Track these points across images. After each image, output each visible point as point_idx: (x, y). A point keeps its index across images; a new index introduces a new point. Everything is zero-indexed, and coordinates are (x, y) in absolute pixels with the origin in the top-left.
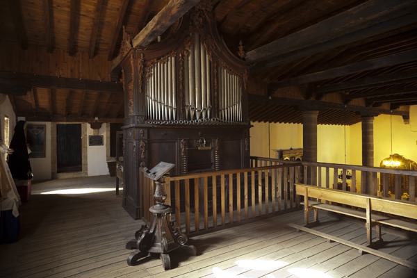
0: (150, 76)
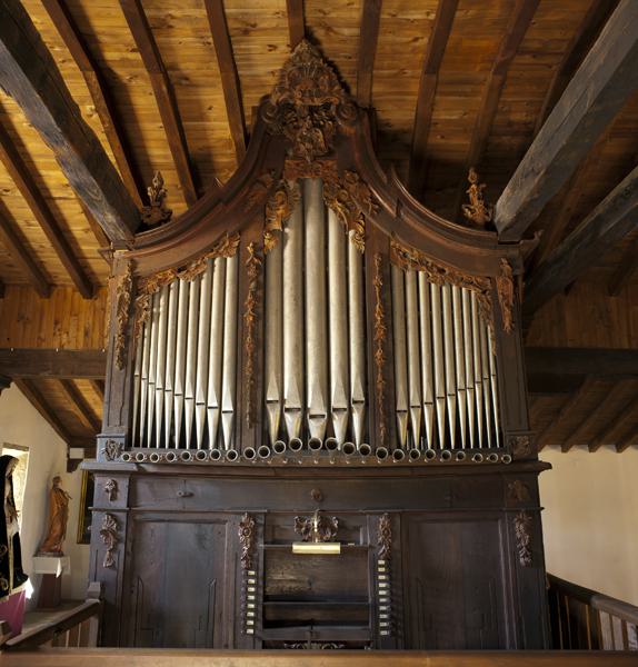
0: (153, 318)
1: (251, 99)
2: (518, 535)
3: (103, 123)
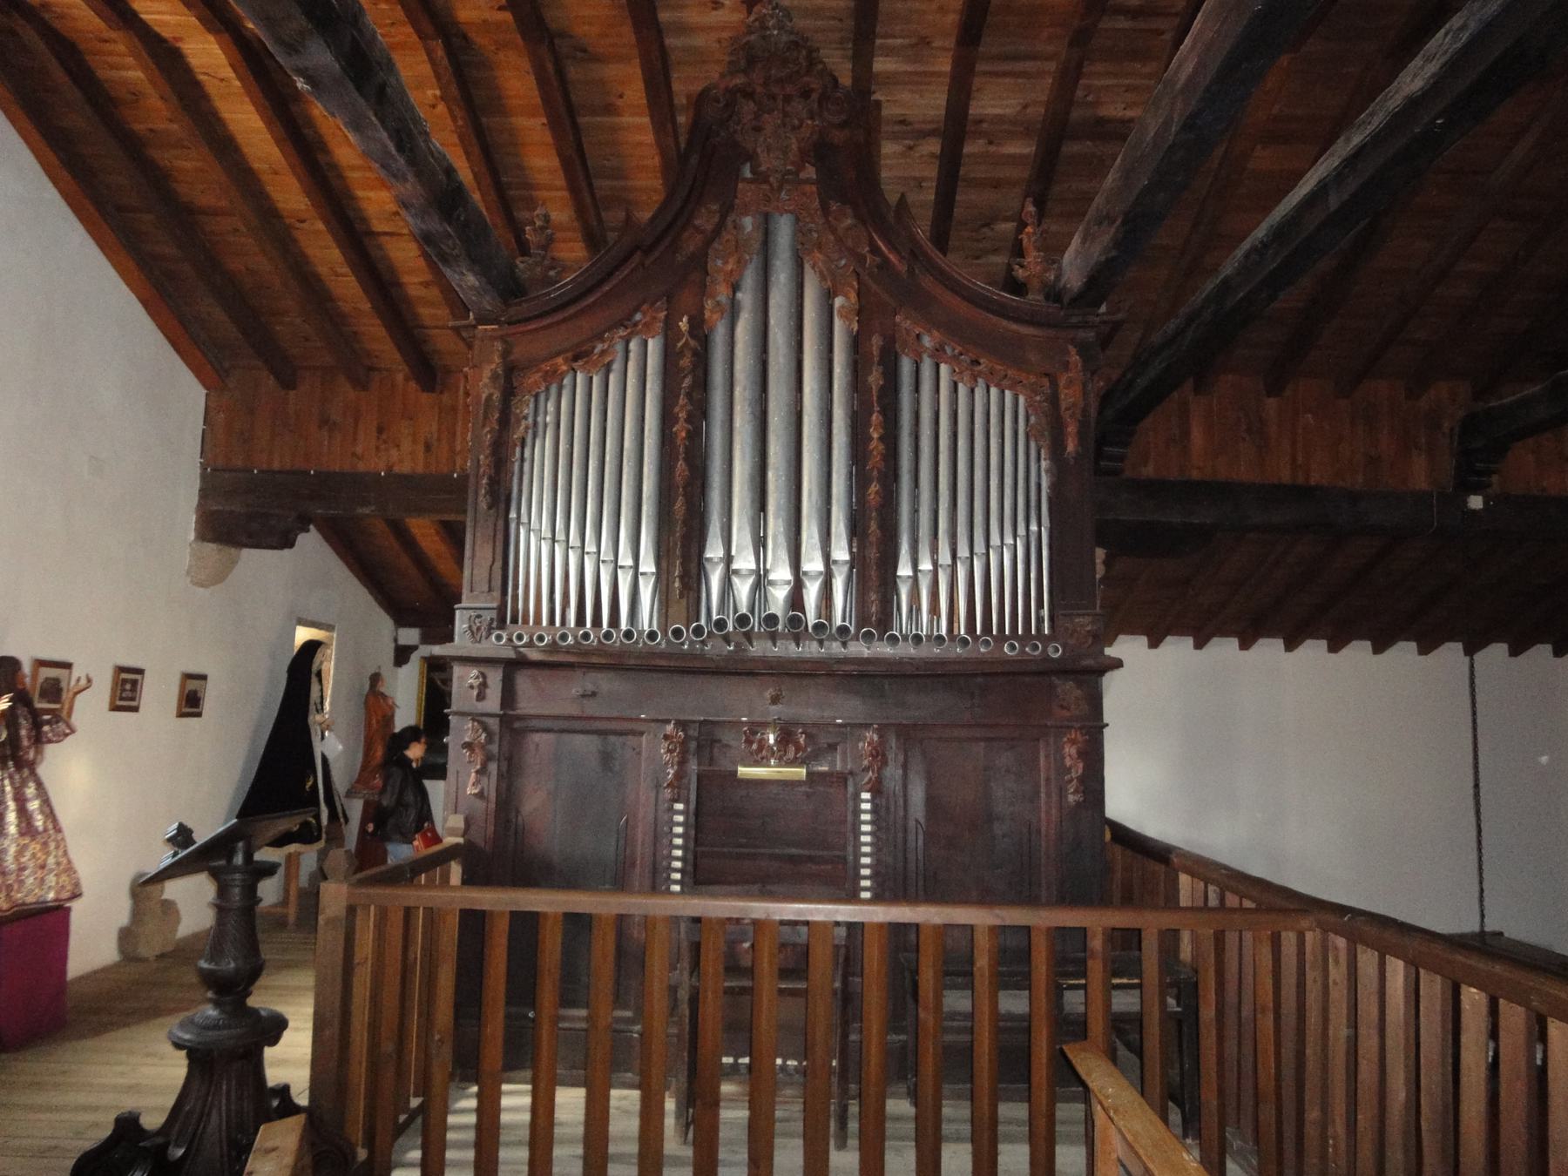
1: (684, 86)
2: (1068, 762)
3: (454, 119)
